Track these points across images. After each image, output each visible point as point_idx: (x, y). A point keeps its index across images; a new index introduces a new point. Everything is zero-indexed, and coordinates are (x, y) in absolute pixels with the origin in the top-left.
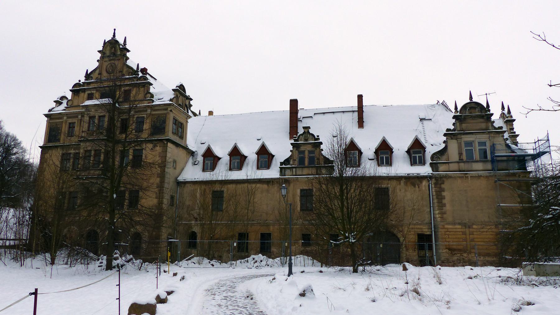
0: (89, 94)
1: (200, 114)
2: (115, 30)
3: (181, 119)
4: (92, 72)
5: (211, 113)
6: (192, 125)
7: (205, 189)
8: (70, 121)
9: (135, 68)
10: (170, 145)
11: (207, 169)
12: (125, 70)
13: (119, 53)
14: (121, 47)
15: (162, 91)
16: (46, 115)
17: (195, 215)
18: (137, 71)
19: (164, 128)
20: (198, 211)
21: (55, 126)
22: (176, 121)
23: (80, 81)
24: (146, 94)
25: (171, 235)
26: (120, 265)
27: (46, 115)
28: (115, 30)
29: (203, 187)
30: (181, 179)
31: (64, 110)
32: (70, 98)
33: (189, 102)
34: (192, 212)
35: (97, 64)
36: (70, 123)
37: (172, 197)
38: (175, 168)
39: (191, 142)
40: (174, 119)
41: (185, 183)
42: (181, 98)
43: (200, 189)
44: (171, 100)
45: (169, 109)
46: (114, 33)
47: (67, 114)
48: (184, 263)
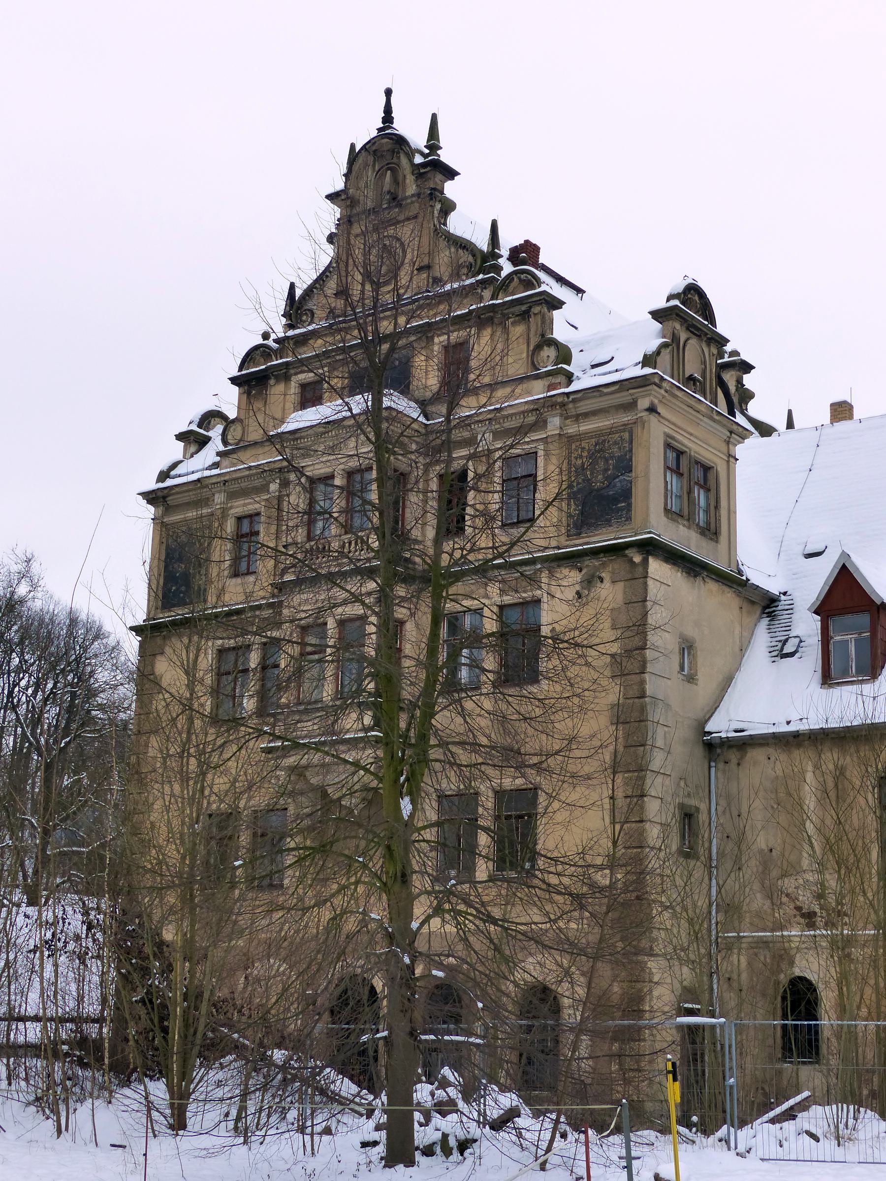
0: (303, 386)
1: (790, 425)
2: (388, 93)
3: (701, 444)
4: (309, 292)
5: (841, 411)
6: (757, 476)
7: (840, 773)
8: (241, 507)
9: (482, 242)
10: (657, 567)
11: (845, 672)
12: (444, 258)
13: (411, 188)
14: (418, 159)
15: (607, 329)
16: (151, 497)
17: (805, 899)
18: (493, 254)
19: (626, 494)
20: (811, 877)
21: (187, 536)
22: (678, 459)
23: (266, 336)
24: (539, 347)
25: (691, 999)
26: (452, 1143)
27: (151, 497)
28: (388, 93)
29: (830, 758)
30: (721, 725)
31: (216, 465)
32: (232, 414)
33: (740, 382)
34: (789, 884)
35: (326, 255)
36: (239, 519)
37: (688, 817)
38: (691, 679)
39: (758, 556)
40: (668, 446)
41: (743, 744)
42: (693, 349)
43: (817, 767)
44: (648, 360)
45: (644, 403)
46: (388, 110)
47: (224, 482)
48: (761, 1134)
